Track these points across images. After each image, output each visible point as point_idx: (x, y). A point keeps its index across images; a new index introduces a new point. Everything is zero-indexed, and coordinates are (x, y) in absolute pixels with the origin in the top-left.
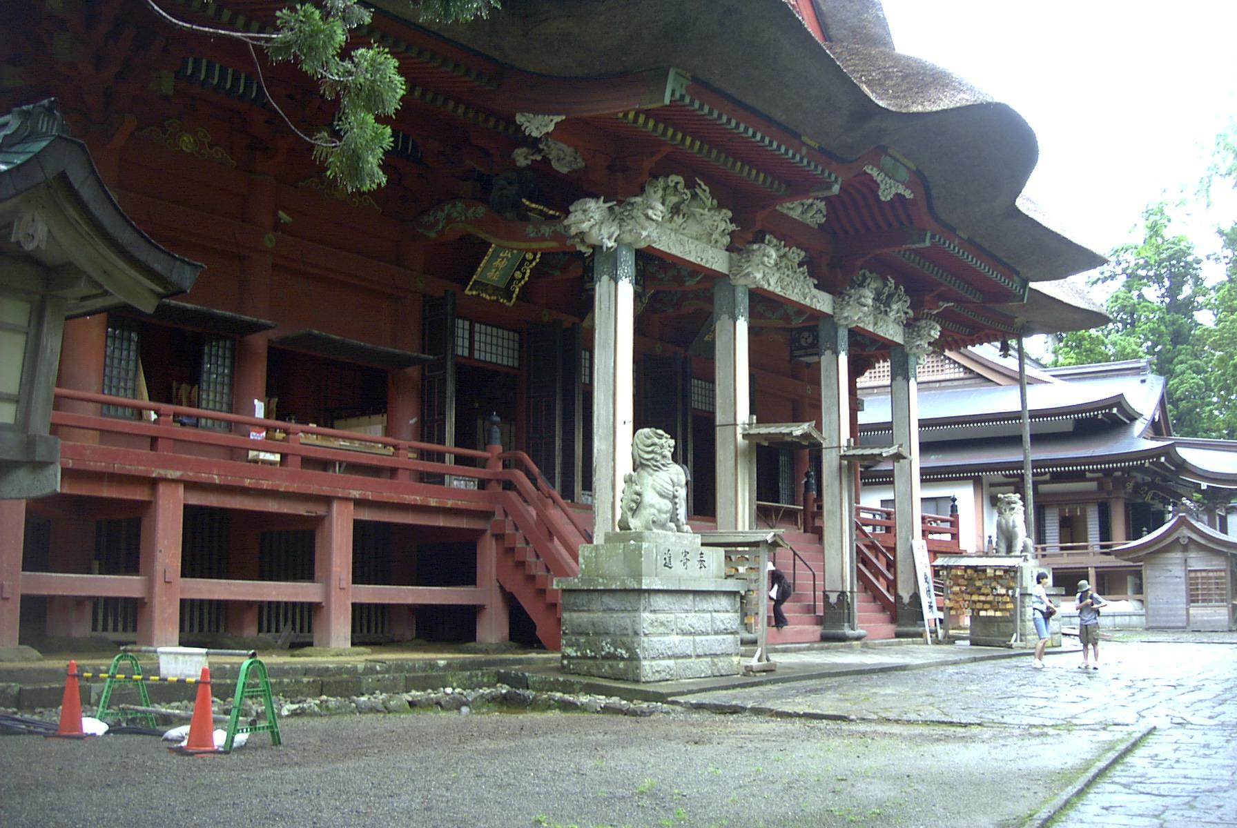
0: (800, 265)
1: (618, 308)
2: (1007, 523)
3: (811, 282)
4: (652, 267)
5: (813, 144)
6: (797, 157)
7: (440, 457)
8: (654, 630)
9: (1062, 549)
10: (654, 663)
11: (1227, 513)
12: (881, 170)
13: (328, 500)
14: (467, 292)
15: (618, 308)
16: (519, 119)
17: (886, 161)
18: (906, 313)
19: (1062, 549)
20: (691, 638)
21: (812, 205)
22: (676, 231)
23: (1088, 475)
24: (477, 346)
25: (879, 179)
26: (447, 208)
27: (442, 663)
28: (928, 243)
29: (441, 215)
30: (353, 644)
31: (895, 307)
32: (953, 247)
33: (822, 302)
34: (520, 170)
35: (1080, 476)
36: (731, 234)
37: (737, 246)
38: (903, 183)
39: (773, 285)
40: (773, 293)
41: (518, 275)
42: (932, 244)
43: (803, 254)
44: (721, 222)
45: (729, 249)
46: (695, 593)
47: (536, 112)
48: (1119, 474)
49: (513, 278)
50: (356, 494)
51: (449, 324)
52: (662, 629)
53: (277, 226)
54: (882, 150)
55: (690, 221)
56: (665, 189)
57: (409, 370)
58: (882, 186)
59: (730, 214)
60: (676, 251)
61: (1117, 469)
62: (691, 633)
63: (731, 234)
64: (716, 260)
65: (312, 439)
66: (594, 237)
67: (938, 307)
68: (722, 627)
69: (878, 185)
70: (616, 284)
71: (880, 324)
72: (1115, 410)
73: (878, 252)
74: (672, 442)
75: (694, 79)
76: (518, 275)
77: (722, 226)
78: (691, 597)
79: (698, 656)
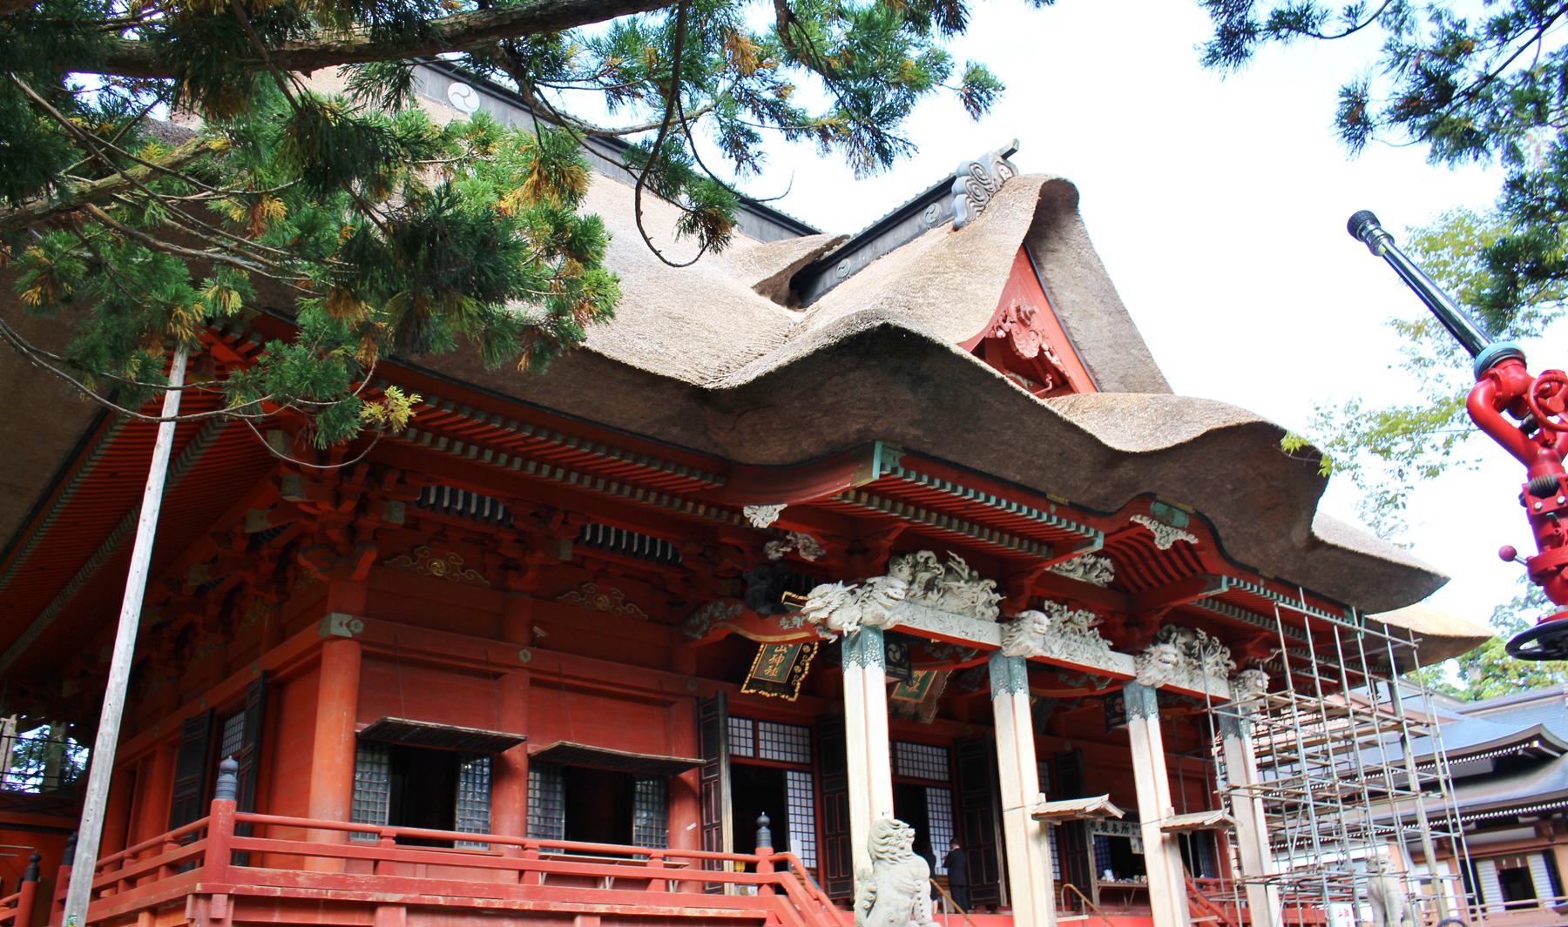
0: (1090, 628)
1: (866, 694)
3: (1105, 644)
4: (905, 649)
5: (1061, 500)
6: (1049, 519)
7: (720, 863)
9: (1508, 908)
12: (1153, 517)
14: (743, 691)
15: (866, 694)
16: (747, 511)
17: (1157, 508)
19: (1508, 908)
21: (1094, 564)
23: (1521, 820)
24: (762, 744)
25: (1152, 528)
26: (710, 608)
28: (1225, 589)
29: (705, 616)
33: (1121, 664)
34: (772, 563)
35: (1511, 822)
36: (999, 604)
37: (1007, 616)
38: (1183, 529)
39: (1059, 651)
41: (798, 669)
42: (1231, 588)
43: (1092, 616)
44: (983, 593)
45: (1000, 620)
47: (760, 504)
48: (1559, 815)
49: (793, 673)
50: (602, 909)
51: (722, 724)
53: (534, 642)
54: (1150, 497)
55: (947, 596)
56: (914, 566)
57: (684, 775)
58: (1158, 535)
59: (994, 584)
61: (1557, 810)
64: (986, 633)
65: (273, 880)
66: (836, 621)
72: (1536, 744)
73: (1176, 604)
74: (912, 831)
75: (906, 449)
76: (798, 669)
77: (984, 597)
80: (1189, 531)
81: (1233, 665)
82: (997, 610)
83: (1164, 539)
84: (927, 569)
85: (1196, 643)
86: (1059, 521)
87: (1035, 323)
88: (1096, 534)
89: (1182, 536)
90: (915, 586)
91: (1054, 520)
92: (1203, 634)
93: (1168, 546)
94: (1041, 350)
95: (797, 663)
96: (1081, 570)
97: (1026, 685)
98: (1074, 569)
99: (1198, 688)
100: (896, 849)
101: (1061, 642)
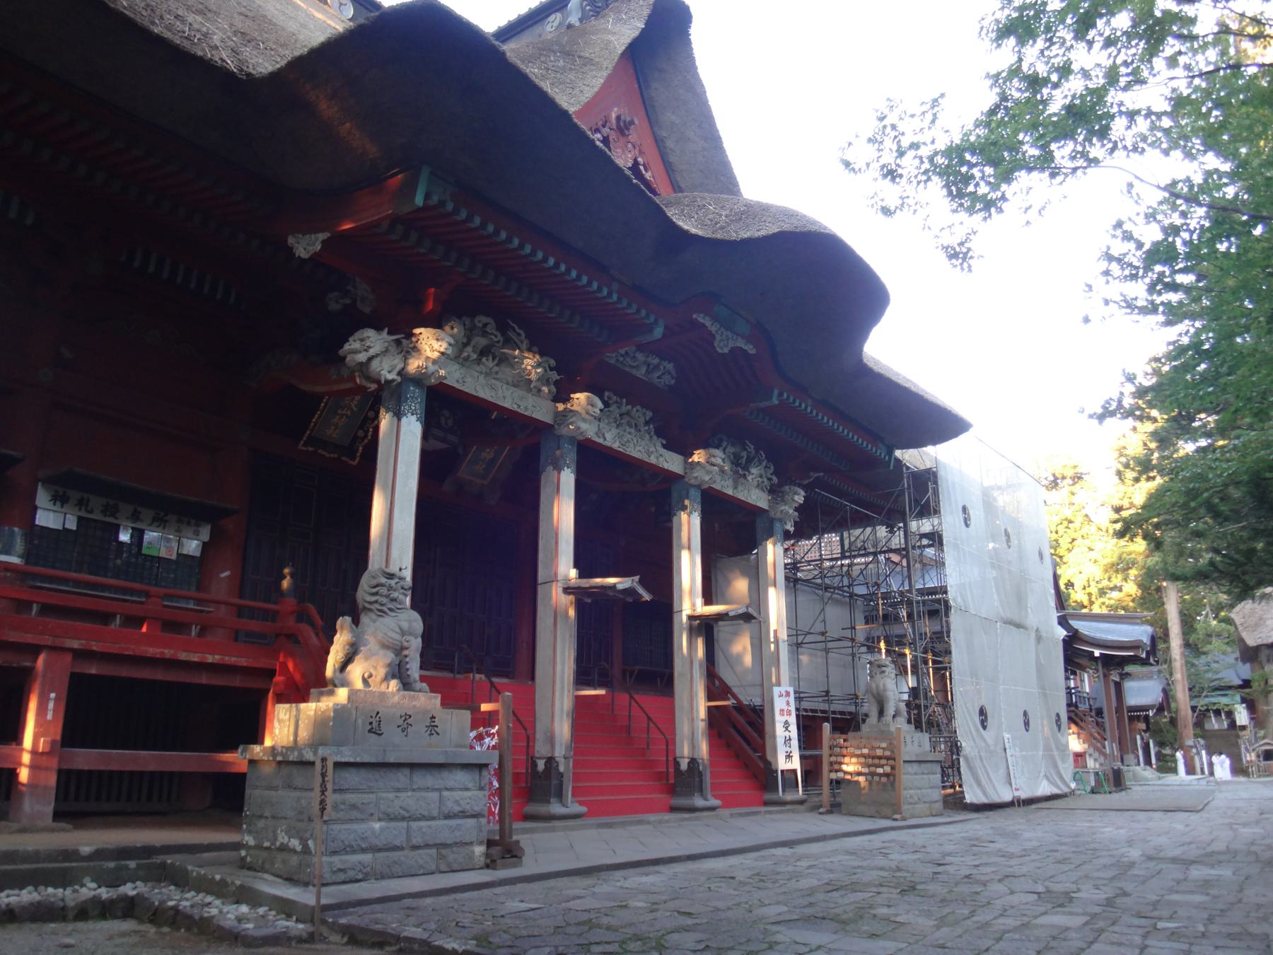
0: (647, 423)
2: (877, 686)
3: (658, 442)
4: (443, 406)
8: (341, 815)
10: (336, 859)
11: (1122, 679)
12: (715, 319)
13: (35, 650)
14: (301, 447)
16: (291, 240)
18: (770, 479)
20: (404, 824)
21: (657, 367)
22: (487, 374)
25: (713, 329)
27: (86, 850)
28: (775, 401)
30: (58, 815)
31: (754, 471)
32: (807, 407)
36: (556, 383)
40: (610, 449)
41: (361, 433)
46: (413, 766)
50: (75, 644)
52: (355, 814)
58: (718, 337)
59: (553, 363)
60: (485, 393)
62: (403, 819)
63: (556, 383)
67: (809, 477)
68: (457, 809)
69: (713, 337)
70: (399, 420)
71: (740, 488)
76: (361, 433)
78: (407, 771)
79: (415, 848)
80: (748, 340)
81: (775, 479)
82: (554, 389)
83: (724, 343)
84: (485, 334)
85: (744, 454)
86: (619, 299)
87: (633, 137)
88: (656, 322)
89: (740, 343)
90: (469, 349)
91: (615, 297)
92: (751, 448)
93: (726, 350)
94: (636, 163)
95: (361, 427)
96: (644, 369)
97: (574, 466)
98: (640, 366)
99: (742, 495)
100: (384, 600)
101: (614, 431)
